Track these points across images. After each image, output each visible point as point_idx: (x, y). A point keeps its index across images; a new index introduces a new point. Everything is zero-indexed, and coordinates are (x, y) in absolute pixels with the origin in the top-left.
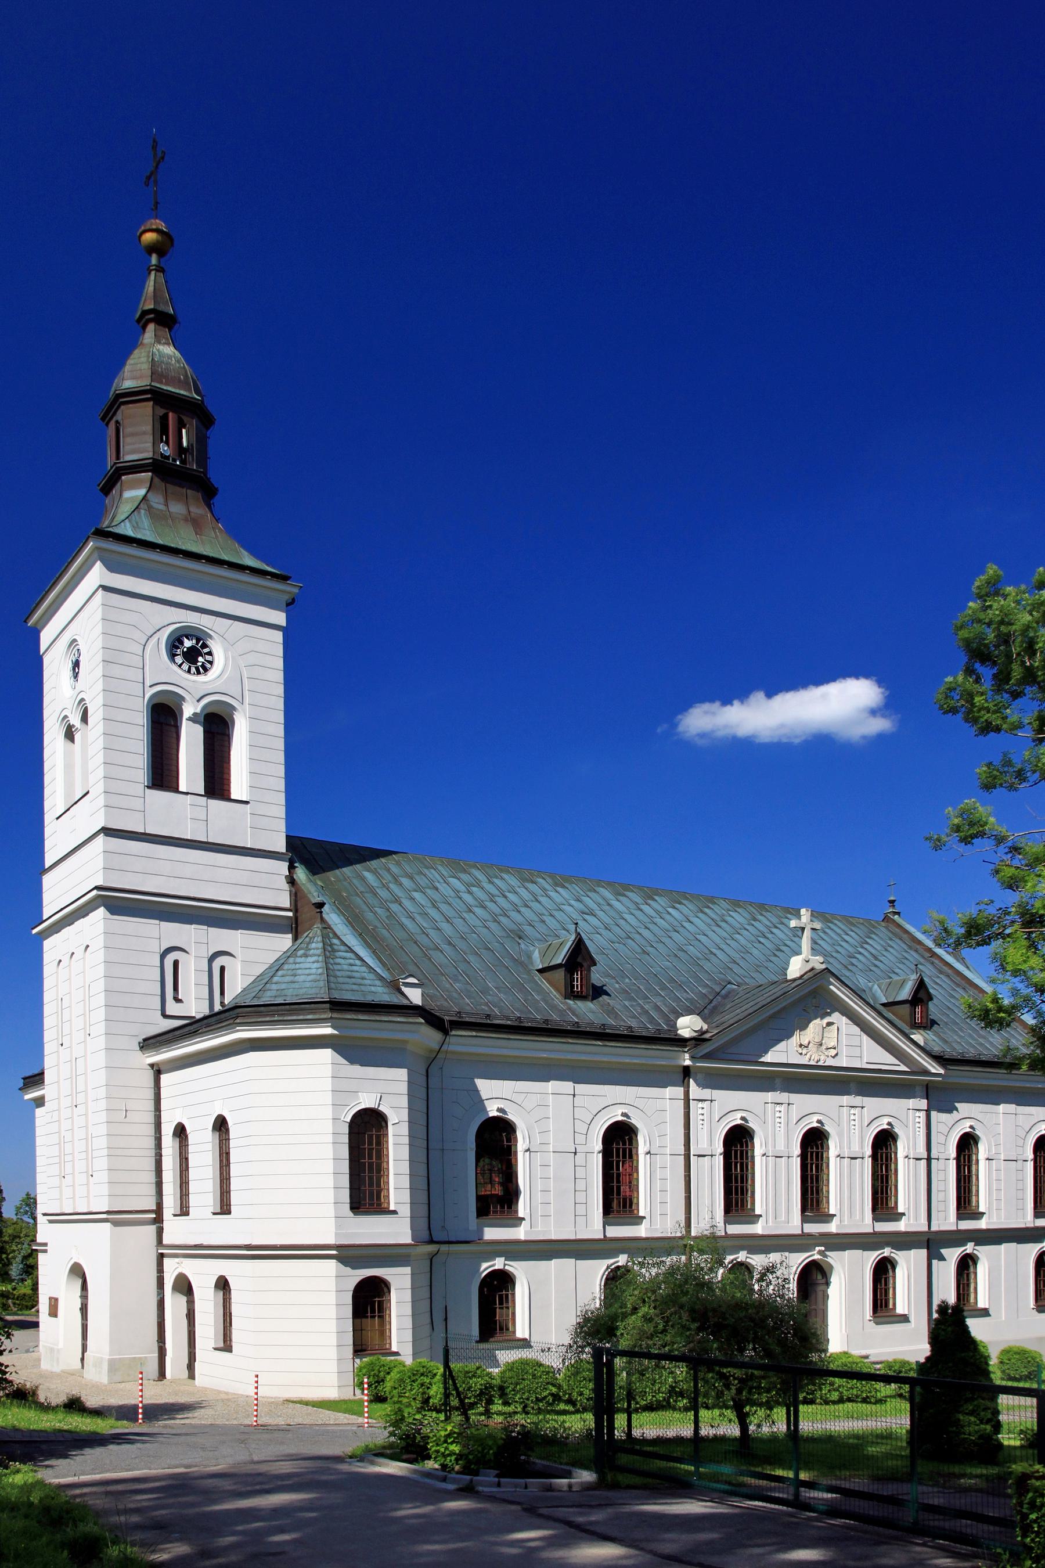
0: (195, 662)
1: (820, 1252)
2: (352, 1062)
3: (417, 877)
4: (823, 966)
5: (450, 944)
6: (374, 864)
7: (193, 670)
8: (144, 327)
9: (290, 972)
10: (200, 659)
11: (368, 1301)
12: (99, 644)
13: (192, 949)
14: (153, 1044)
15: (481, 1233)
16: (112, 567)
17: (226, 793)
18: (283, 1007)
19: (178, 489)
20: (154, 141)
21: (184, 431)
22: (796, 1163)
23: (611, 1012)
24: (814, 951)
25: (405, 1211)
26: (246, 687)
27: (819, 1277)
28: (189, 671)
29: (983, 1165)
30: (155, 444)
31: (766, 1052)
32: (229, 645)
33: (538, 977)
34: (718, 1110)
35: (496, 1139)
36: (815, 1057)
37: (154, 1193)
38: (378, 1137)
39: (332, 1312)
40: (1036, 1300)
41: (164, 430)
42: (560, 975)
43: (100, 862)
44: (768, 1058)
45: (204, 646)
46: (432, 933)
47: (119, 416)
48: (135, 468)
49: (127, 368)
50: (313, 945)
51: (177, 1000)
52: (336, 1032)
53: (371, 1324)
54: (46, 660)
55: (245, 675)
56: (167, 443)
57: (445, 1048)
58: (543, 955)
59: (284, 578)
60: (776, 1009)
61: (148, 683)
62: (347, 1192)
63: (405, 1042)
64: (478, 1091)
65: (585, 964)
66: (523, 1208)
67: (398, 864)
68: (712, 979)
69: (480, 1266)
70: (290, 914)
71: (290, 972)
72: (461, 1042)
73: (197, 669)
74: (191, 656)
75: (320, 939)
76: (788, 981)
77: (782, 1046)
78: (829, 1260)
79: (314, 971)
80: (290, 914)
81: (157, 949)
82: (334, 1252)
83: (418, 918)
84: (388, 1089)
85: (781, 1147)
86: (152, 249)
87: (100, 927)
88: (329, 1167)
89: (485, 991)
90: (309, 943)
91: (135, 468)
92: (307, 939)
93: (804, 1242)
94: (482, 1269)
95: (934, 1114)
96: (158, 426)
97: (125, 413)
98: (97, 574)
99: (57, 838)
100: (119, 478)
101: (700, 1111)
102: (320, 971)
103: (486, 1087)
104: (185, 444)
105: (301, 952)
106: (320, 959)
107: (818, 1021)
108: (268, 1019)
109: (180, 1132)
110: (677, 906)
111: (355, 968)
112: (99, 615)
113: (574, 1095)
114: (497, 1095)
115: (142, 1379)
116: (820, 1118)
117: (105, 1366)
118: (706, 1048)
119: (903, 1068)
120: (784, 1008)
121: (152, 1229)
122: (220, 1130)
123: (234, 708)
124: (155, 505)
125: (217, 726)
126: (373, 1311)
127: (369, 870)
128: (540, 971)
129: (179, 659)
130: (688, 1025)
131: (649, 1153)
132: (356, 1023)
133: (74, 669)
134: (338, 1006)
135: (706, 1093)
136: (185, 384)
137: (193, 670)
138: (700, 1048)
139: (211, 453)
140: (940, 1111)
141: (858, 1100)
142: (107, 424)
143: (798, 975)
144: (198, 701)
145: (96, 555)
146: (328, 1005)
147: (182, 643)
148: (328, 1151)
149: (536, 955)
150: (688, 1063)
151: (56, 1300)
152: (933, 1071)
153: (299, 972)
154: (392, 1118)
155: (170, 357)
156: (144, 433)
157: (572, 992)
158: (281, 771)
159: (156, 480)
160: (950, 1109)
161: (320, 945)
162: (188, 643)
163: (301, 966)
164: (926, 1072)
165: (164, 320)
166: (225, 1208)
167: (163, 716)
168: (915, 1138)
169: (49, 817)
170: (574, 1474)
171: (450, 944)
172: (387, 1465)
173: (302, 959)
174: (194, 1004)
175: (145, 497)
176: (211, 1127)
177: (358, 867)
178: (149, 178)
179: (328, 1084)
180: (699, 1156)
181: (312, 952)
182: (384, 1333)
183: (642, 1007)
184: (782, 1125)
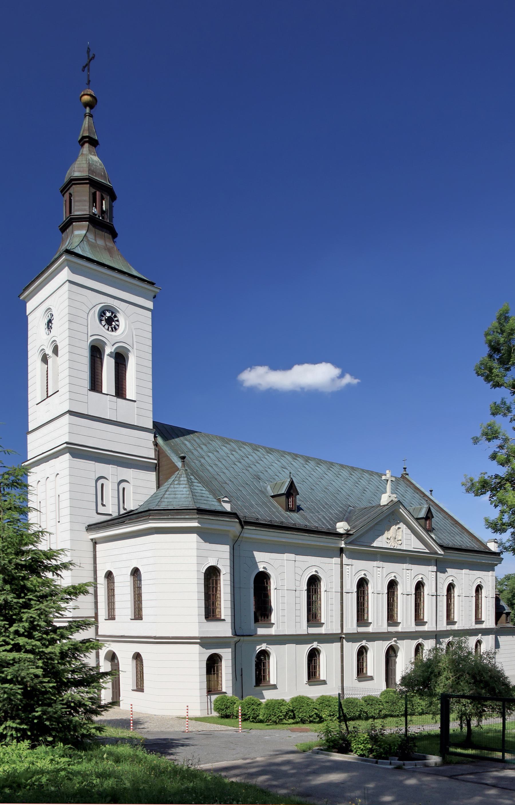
0: (111, 325)
1: (395, 641)
2: (206, 541)
3: (208, 445)
4: (396, 500)
5: (231, 481)
6: (188, 437)
7: (110, 329)
8: (82, 145)
9: (173, 493)
10: (113, 323)
11: (213, 664)
12: (66, 311)
14: (94, 528)
15: (256, 631)
16: (74, 271)
17: (124, 395)
18: (173, 511)
19: (100, 232)
20: (88, 48)
21: (104, 202)
22: (386, 596)
23: (306, 519)
25: (229, 619)
27: (393, 653)
28: (108, 330)
29: (456, 598)
30: (90, 209)
31: (374, 542)
33: (272, 499)
34: (356, 568)
35: (262, 580)
36: (393, 545)
37: (94, 608)
38: (216, 581)
41: (94, 201)
43: (66, 429)
44: (375, 544)
45: (115, 316)
46: (221, 474)
47: (71, 191)
48: (80, 219)
49: (76, 166)
50: (182, 479)
51: (103, 505)
53: (213, 677)
54: (30, 319)
55: (134, 334)
56: (96, 207)
57: (242, 535)
58: (273, 488)
59: (153, 284)
60: (378, 521)
61: (89, 335)
63: (228, 531)
64: (254, 558)
65: (294, 494)
66: (273, 618)
67: (198, 437)
68: (342, 504)
69: (256, 648)
70: (156, 462)
71: (173, 493)
72: (250, 532)
73: (112, 328)
74: (109, 321)
75: (185, 476)
77: (380, 539)
78: (398, 644)
79: (185, 492)
80: (156, 462)
82: (199, 641)
83: (214, 467)
84: (220, 556)
85: (379, 589)
86: (87, 104)
87: (66, 464)
88: (195, 596)
89: (252, 506)
90: (179, 478)
91: (80, 219)
92: (178, 475)
93: (389, 636)
94: (257, 649)
95: (438, 573)
97: (75, 189)
98: (65, 274)
99: (36, 415)
100: (71, 223)
102: (188, 493)
103: (259, 556)
104: (104, 209)
105: (176, 482)
107: (394, 527)
108: (166, 517)
109: (109, 575)
110: (319, 466)
114: (264, 560)
116: (365, 572)
118: (351, 538)
119: (427, 551)
120: (381, 520)
122: (134, 575)
123: (129, 351)
124: (90, 240)
125: (120, 360)
126: (214, 671)
127: (187, 440)
128: (272, 497)
129: (104, 323)
131: (276, 589)
132: (209, 521)
135: (350, 561)
136: (104, 177)
137: (110, 329)
139: (114, 215)
140: (441, 572)
141: (409, 566)
142: (63, 195)
143: (386, 503)
144: (113, 345)
145: (66, 263)
146: (196, 511)
147: (105, 314)
149: (269, 488)
150: (343, 546)
152: (439, 553)
153: (177, 493)
154: (223, 572)
155: (96, 162)
156: (85, 201)
157: (289, 508)
159: (91, 226)
160: (444, 572)
161: (186, 479)
162: (108, 314)
164: (436, 553)
165: (94, 143)
166: (138, 615)
167: (96, 352)
168: (431, 585)
169: (31, 403)
170: (427, 758)
171: (231, 481)
172: (336, 756)
173: (177, 486)
174: (111, 509)
176: (129, 574)
177: (182, 438)
178: (84, 67)
179: (195, 553)
180: (347, 593)
181: (182, 482)
182: (218, 682)
183: (318, 517)
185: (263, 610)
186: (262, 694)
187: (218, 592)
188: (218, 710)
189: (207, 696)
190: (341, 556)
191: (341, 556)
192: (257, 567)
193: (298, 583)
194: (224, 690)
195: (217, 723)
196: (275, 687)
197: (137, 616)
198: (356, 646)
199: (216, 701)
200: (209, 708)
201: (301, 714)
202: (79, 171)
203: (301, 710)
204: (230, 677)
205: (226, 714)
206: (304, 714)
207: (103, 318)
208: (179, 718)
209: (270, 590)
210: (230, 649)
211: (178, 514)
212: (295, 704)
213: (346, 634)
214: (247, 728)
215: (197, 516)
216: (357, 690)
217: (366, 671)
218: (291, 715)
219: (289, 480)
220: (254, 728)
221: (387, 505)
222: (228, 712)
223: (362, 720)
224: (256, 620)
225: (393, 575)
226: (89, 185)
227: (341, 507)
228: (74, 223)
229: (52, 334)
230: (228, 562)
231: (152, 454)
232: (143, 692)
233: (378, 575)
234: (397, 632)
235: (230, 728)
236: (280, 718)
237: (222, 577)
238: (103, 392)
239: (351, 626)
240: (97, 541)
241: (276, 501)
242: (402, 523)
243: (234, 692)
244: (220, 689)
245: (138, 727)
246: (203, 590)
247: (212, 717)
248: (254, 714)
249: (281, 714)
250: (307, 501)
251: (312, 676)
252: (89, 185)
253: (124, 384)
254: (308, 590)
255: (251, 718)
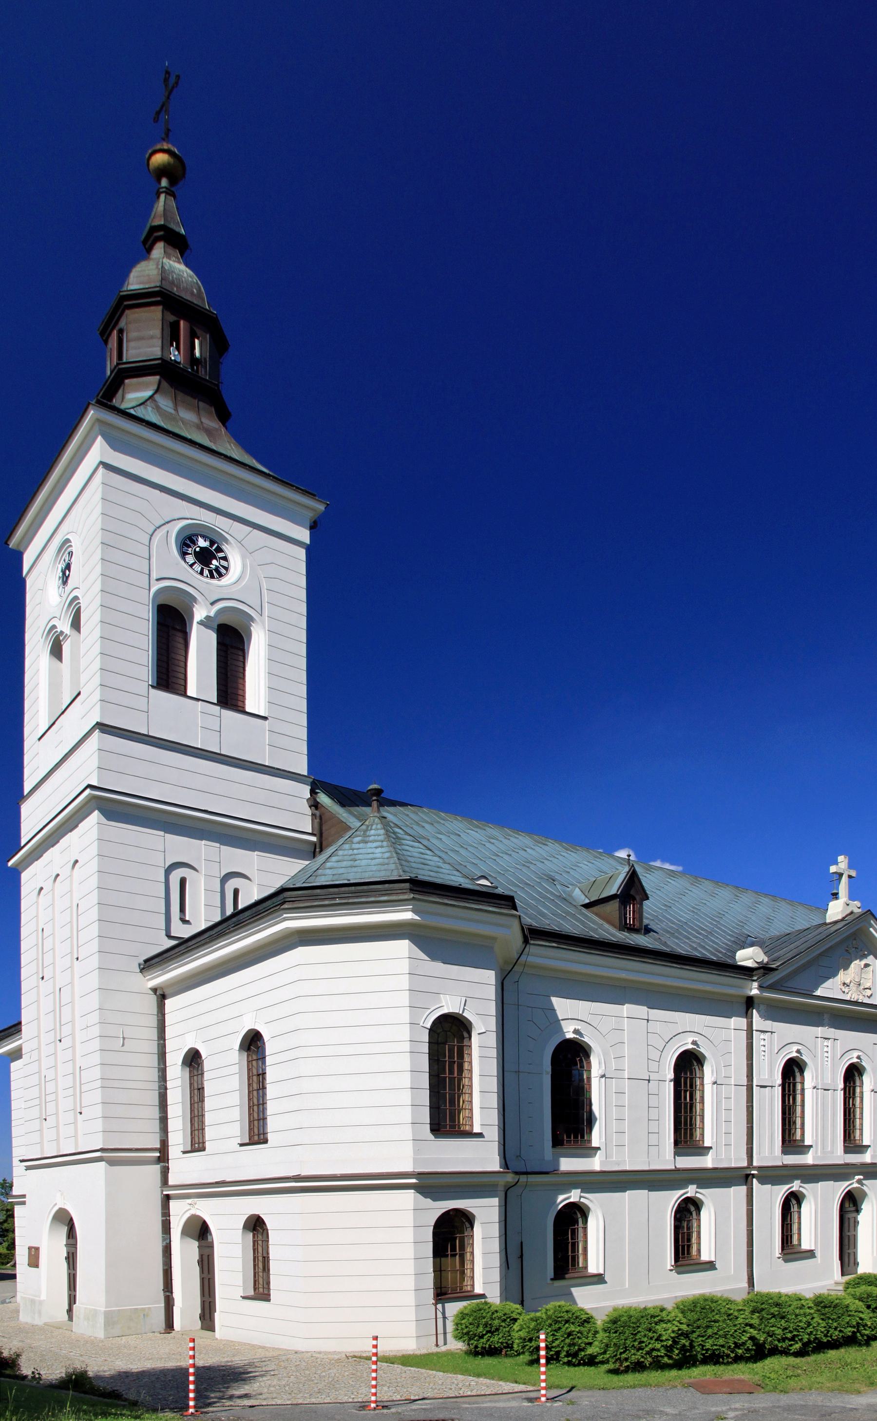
1: (859, 1181)
7: (206, 572)
10: (214, 562)
13: (202, 866)
16: (115, 444)
18: (343, 889)
21: (197, 341)
24: (852, 897)
25: (493, 1134)
26: (266, 599)
28: (201, 573)
31: (817, 989)
32: (247, 552)
33: (584, 910)
34: (778, 1040)
35: (571, 1057)
37: (157, 1129)
39: (409, 1251)
40: (783, 1249)
42: (615, 905)
43: (94, 763)
45: (219, 550)
47: (122, 324)
48: (141, 370)
52: (417, 918)
55: (265, 586)
60: (824, 948)
61: (154, 576)
62: (427, 1110)
63: (494, 939)
65: (638, 898)
66: (597, 1137)
70: (314, 839)
72: (543, 956)
73: (210, 572)
74: (204, 557)
76: (825, 924)
77: (829, 983)
78: (865, 1188)
79: (379, 855)
80: (314, 839)
81: (161, 862)
82: (414, 1181)
86: (163, 171)
87: (94, 834)
90: (367, 830)
91: (141, 370)
94: (559, 1200)
96: (168, 331)
98: (99, 450)
99: (36, 759)
101: (762, 1043)
103: (563, 1006)
106: (385, 844)
107: (857, 962)
108: (327, 902)
109: (193, 1059)
111: (426, 857)
112: (99, 495)
113: (648, 1020)
114: (574, 1016)
115: (193, 1349)
116: (800, 1047)
117: (101, 1320)
118: (773, 978)
120: (831, 947)
121: (157, 1168)
122: (248, 1049)
123: (252, 619)
125: (232, 641)
126: (453, 1249)
128: (587, 906)
129: (190, 559)
130: (748, 957)
131: (715, 1083)
133: (64, 573)
134: (421, 888)
135: (768, 1025)
137: (206, 572)
138: (768, 977)
143: (840, 917)
144: (212, 604)
145: (97, 428)
146: (407, 885)
148: (405, 1062)
149: (577, 893)
150: (755, 992)
151: (37, 1249)
153: (360, 856)
156: (152, 337)
158: (303, 690)
159: (165, 384)
161: (382, 832)
162: (202, 543)
163: (361, 851)
166: (257, 1134)
167: (171, 621)
173: (361, 845)
175: (151, 397)
179: (404, 982)
181: (372, 838)
182: (463, 1271)
184: (829, 1059)
185: (572, 1118)
186: (571, 1294)
187: (465, 1073)
188: (466, 1338)
189: (436, 1305)
190: (747, 1014)
191: (747, 1014)
192: (559, 1029)
193: (654, 1066)
194: (478, 1290)
195: (466, 1372)
196: (599, 1279)
197: (256, 1138)
198: (781, 1191)
199: (462, 1315)
200: (440, 1330)
201: (710, 1341)
202: (141, 283)
203: (710, 1332)
204: (496, 1260)
205: (486, 1341)
206: (721, 1341)
207: (190, 550)
208: (359, 1358)
209: (589, 1078)
210: (497, 1199)
211: (357, 894)
212: (693, 1316)
213: (760, 1168)
214: (558, 1387)
215: (412, 896)
216: (782, 1280)
217: (799, 1239)
218: (684, 1345)
219: (627, 869)
220: (579, 1385)
221: (843, 919)
222: (496, 1340)
223: (860, 1345)
224: (557, 1142)
225: (855, 1054)
226: (160, 308)
227: (730, 935)
228: (127, 381)
229: (69, 587)
230: (491, 1008)
231: (307, 825)
232: (269, 1300)
233: (826, 1054)
234: (864, 1165)
235: (507, 1387)
236: (654, 1354)
237: (475, 1040)
238: (189, 694)
239: (769, 1151)
240: (167, 992)
241: (596, 914)
242: (871, 957)
243: (506, 1294)
244: (469, 1288)
245: (237, 1393)
246: (425, 1097)
247: (449, 1354)
248: (570, 1345)
249: (658, 1346)
250: (660, 920)
251: (683, 1254)
252: (160, 308)
253: (241, 686)
254: (677, 1081)
255: (563, 1354)
